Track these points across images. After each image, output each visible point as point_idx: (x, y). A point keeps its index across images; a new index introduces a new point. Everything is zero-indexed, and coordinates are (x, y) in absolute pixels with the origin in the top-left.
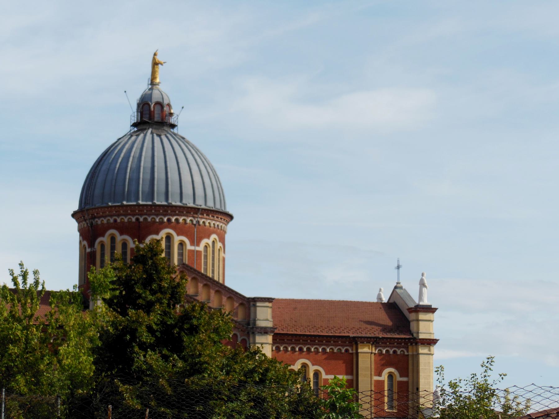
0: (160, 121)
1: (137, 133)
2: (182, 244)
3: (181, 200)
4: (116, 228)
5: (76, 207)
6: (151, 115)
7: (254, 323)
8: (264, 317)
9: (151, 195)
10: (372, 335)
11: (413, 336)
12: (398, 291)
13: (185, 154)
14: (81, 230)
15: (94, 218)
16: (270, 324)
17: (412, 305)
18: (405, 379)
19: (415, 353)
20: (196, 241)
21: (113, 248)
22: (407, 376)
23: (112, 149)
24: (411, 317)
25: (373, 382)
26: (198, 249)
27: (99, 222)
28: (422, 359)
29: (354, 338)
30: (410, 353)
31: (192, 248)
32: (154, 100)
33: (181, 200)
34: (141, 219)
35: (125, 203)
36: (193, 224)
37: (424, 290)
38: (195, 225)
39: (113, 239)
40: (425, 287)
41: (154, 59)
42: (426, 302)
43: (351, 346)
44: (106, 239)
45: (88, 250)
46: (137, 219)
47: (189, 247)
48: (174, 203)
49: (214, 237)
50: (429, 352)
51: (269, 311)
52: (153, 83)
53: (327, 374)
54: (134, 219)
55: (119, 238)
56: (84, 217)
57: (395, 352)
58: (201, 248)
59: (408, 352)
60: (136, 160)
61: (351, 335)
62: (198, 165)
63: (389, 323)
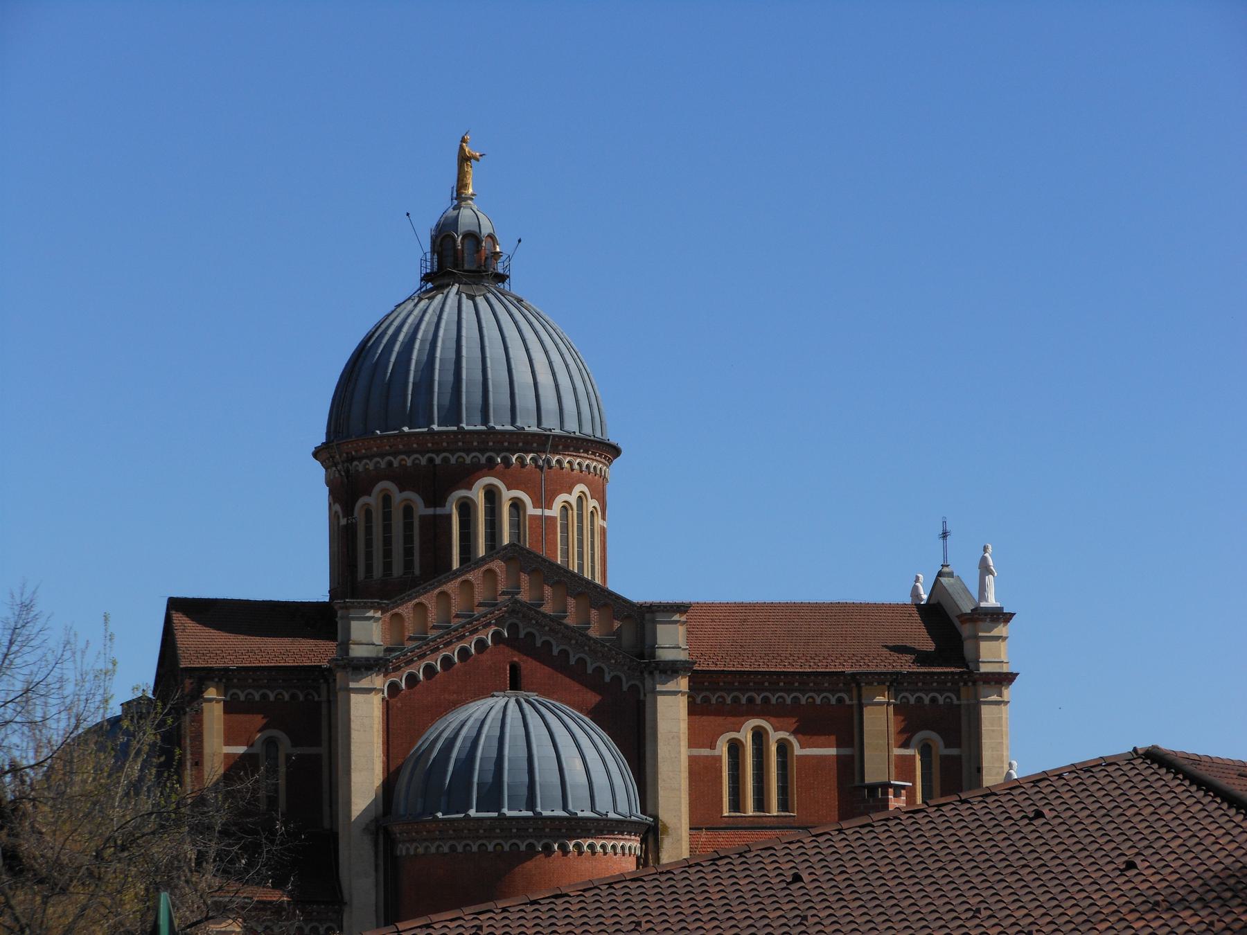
0: (474, 268)
1: (427, 294)
2: (517, 505)
3: (513, 422)
4: (388, 478)
5: (320, 438)
6: (457, 260)
7: (653, 655)
8: (672, 641)
9: (453, 412)
10: (891, 669)
11: (968, 667)
12: (945, 580)
13: (520, 331)
14: (329, 482)
15: (351, 459)
16: (682, 656)
17: (967, 608)
18: (954, 752)
19: (973, 702)
20: (544, 501)
21: (387, 516)
22: (959, 745)
23: (384, 326)
24: (965, 630)
25: (892, 759)
26: (548, 513)
27: (361, 468)
28: (986, 711)
29: (853, 675)
30: (964, 702)
31: (538, 512)
32: (462, 228)
33: (513, 422)
34: (438, 461)
35: (406, 429)
36: (537, 466)
37: (990, 579)
38: (541, 468)
39: (387, 500)
40: (992, 573)
41: (462, 149)
42: (992, 601)
43: (849, 691)
44: (372, 500)
45: (343, 522)
46: (431, 460)
47: (531, 510)
48: (498, 427)
49: (580, 488)
50: (999, 699)
51: (681, 630)
52: (460, 196)
53: (802, 747)
54: (424, 461)
55: (398, 497)
56: (333, 457)
57: (933, 700)
58: (555, 511)
59: (959, 699)
60: (428, 347)
61: (848, 670)
62: (546, 352)
63: (930, 646)
